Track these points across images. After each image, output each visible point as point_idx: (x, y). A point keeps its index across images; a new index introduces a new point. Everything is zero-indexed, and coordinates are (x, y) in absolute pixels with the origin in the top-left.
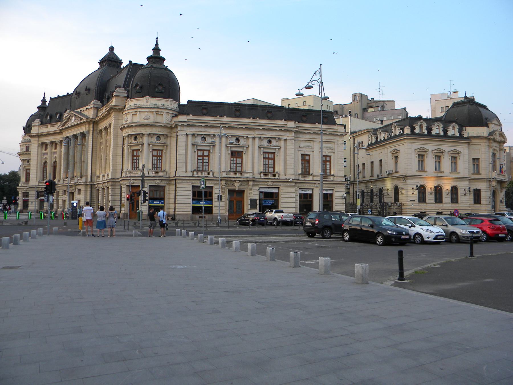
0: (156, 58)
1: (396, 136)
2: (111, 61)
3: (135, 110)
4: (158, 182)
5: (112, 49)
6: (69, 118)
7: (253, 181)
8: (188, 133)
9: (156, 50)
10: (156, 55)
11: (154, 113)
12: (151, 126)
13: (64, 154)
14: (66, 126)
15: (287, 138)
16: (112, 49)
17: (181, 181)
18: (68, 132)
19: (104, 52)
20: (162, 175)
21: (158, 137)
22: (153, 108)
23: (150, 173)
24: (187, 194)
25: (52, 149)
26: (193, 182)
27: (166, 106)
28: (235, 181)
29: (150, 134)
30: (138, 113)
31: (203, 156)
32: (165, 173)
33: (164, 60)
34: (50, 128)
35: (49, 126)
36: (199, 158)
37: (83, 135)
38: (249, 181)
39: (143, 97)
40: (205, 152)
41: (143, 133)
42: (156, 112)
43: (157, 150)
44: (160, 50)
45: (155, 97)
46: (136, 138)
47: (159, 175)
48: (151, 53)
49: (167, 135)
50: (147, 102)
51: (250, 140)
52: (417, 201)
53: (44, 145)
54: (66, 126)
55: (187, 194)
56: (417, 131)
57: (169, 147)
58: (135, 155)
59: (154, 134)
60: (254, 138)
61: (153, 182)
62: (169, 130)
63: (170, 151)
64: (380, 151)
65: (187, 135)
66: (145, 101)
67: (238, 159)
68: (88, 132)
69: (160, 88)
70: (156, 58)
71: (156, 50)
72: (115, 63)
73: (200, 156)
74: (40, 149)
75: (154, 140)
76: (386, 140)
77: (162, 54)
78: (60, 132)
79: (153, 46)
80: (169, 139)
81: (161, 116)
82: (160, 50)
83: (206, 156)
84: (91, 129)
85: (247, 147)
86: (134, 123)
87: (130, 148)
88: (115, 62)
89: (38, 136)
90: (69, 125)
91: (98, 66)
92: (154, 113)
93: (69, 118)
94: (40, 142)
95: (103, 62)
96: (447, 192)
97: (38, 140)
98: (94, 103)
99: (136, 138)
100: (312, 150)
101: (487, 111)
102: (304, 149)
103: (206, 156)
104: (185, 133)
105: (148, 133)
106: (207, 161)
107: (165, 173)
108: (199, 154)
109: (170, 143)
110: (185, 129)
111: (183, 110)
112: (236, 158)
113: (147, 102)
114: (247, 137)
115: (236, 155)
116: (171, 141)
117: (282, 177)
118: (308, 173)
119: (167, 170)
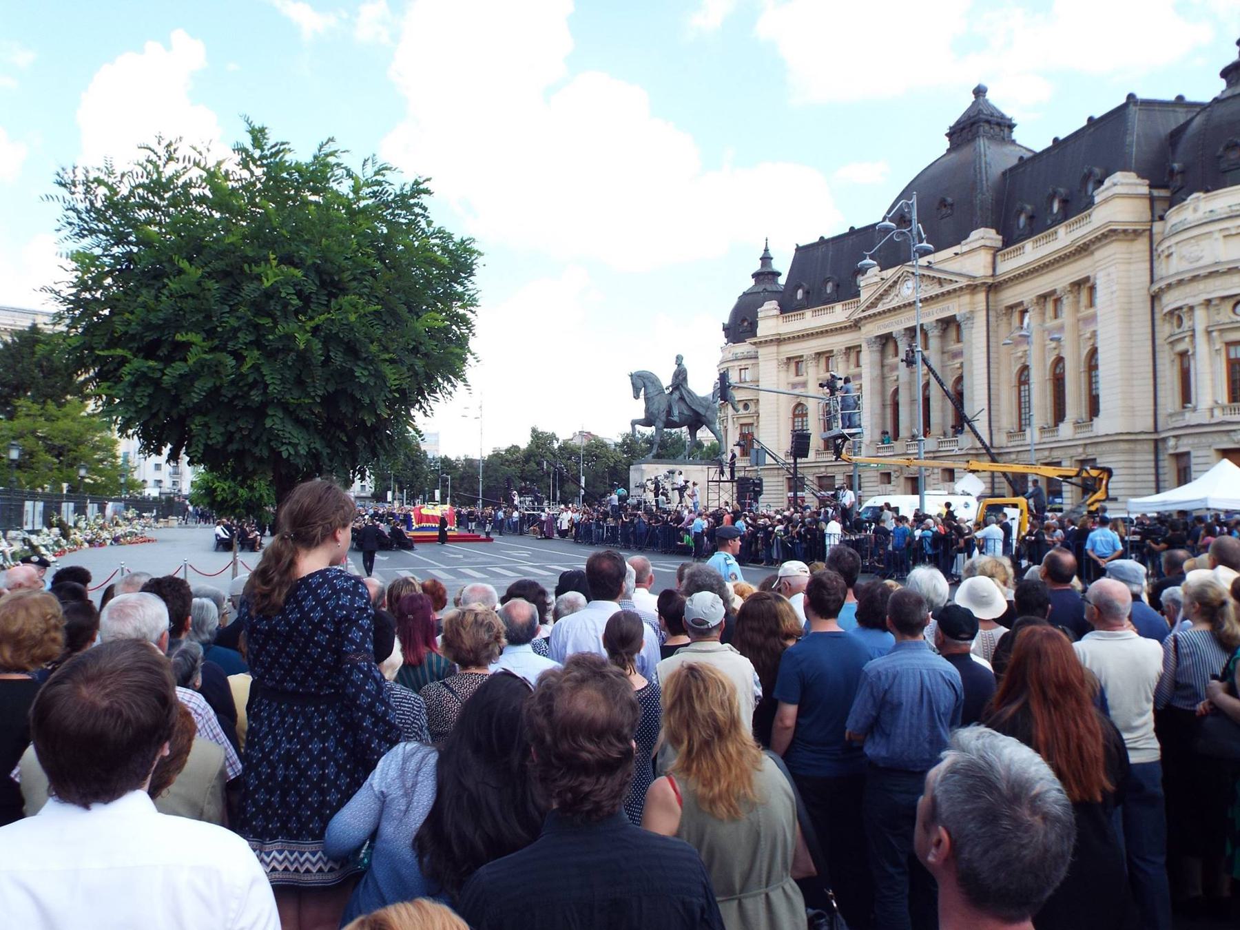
2: (979, 125)
4: (823, 469)
5: (979, 92)
6: (895, 282)
10: (764, 270)
11: (1217, 235)
13: (872, 380)
14: (880, 308)
16: (979, 92)
18: (886, 321)
23: (1217, 412)
24: (1144, 485)
25: (848, 368)
34: (810, 320)
35: (808, 313)
37: (948, 324)
53: (796, 362)
54: (880, 308)
55: (1144, 485)
58: (415, 430)
59: (1223, 298)
60: (1191, 308)
61: (1225, 438)
68: (970, 317)
72: (997, 129)
78: (856, 325)
85: (1193, 336)
86: (1172, 276)
88: (999, 124)
89: (779, 341)
90: (895, 304)
91: (946, 144)
93: (895, 282)
94: (784, 357)
95: (963, 129)
98: (985, 236)
101: (1012, 148)
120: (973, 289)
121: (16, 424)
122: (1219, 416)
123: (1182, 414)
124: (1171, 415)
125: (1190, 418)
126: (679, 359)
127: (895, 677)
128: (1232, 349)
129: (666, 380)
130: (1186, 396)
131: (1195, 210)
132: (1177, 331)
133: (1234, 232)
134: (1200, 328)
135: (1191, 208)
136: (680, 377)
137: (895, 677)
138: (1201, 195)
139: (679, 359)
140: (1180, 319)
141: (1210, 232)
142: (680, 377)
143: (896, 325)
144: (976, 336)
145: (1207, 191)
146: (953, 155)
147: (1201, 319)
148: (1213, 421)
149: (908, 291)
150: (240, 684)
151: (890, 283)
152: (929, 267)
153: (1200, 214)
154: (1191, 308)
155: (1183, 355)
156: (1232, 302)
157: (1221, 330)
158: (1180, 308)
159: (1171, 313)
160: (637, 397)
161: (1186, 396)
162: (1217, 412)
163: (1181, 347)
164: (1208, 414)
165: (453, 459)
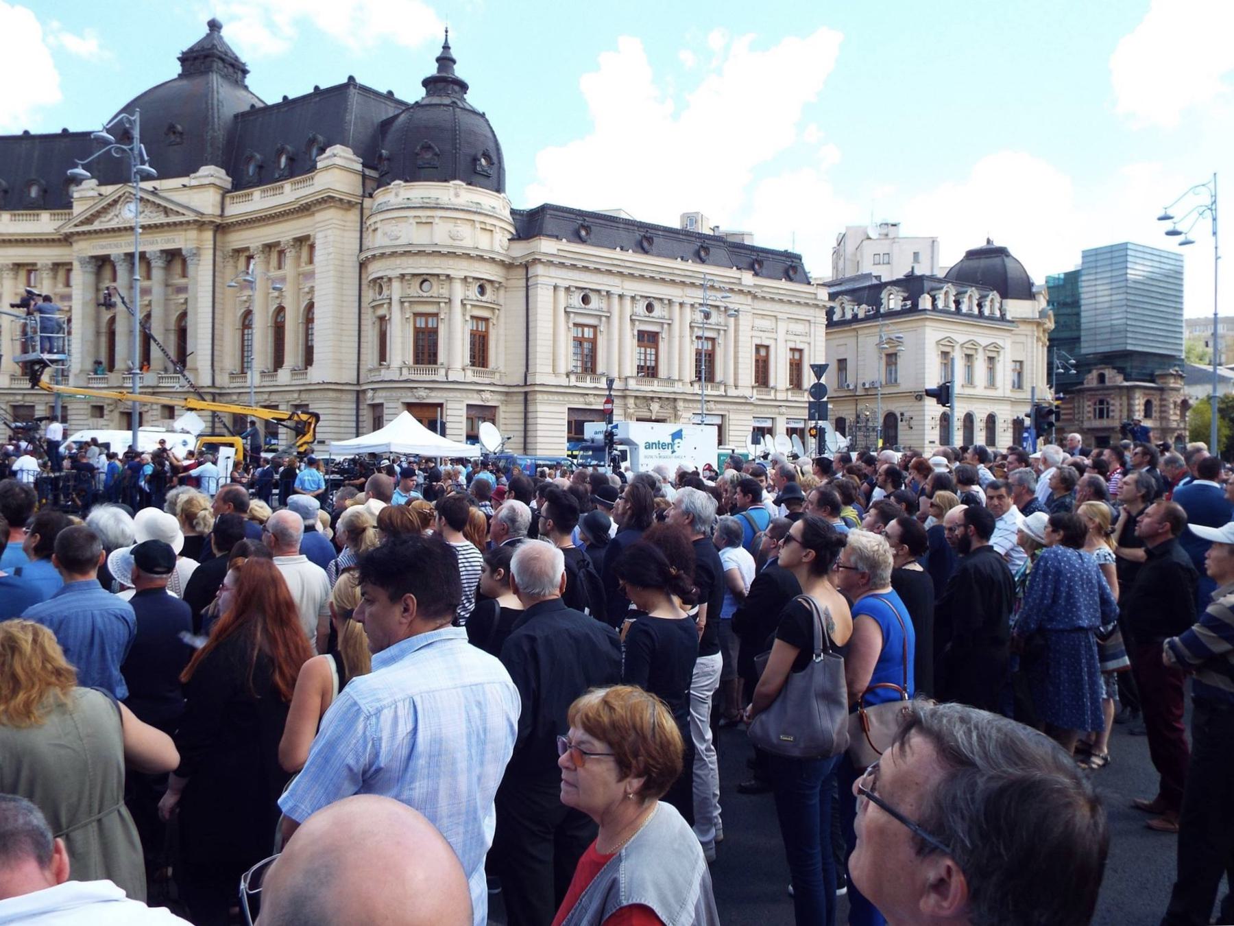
0: (444, 82)
1: (892, 314)
3: (429, 213)
5: (214, 26)
6: (115, 202)
7: (685, 400)
8: (559, 283)
9: (445, 61)
10: (444, 74)
11: (411, 220)
12: (429, 254)
13: (85, 304)
14: (96, 225)
15: (742, 308)
16: (214, 26)
17: (546, 396)
18: (104, 242)
19: (195, 34)
21: (424, 279)
23: (405, 371)
26: (571, 398)
28: (652, 398)
29: (403, 276)
30: (378, 225)
32: (497, 375)
33: (463, 87)
37: (172, 256)
38: (675, 400)
39: (446, 181)
40: (430, 320)
41: (390, 273)
43: (583, 326)
44: (454, 62)
46: (482, 290)
47: (487, 381)
48: (432, 70)
50: (457, 195)
51: (676, 308)
52: (937, 442)
54: (96, 225)
56: (940, 305)
59: (414, 275)
60: (390, 279)
64: (842, 341)
65: (555, 288)
66: (452, 192)
67: (648, 350)
68: (197, 253)
69: (428, 156)
70: (444, 82)
71: (445, 61)
72: (231, 70)
75: (473, 292)
76: (862, 320)
77: (460, 71)
79: (438, 52)
81: (428, 227)
82: (454, 62)
84: (210, 244)
85: (390, 304)
88: (232, 65)
90: (114, 224)
91: (177, 69)
93: (115, 202)
95: (195, 58)
96: (933, 423)
100: (774, 335)
102: (761, 334)
104: (554, 282)
105: (462, 274)
107: (442, 372)
110: (553, 271)
111: (530, 224)
112: (645, 348)
113: (457, 195)
114: (448, 276)
115: (648, 339)
117: (732, 392)
118: (710, 378)
120: (200, 225)
121: (484, 299)
122: (406, 375)
123: (379, 370)
124: (370, 370)
125: (386, 375)
128: (418, 319)
134: (395, 298)
140: (381, 287)
143: (116, 248)
144: (202, 274)
145: (406, 181)
146: (184, 82)
147: (396, 290)
149: (128, 213)
151: (157, 201)
152: (154, 192)
153: (400, 199)
154: (390, 279)
155: (382, 319)
158: (381, 278)
161: (383, 356)
162: (405, 371)
163: (381, 312)
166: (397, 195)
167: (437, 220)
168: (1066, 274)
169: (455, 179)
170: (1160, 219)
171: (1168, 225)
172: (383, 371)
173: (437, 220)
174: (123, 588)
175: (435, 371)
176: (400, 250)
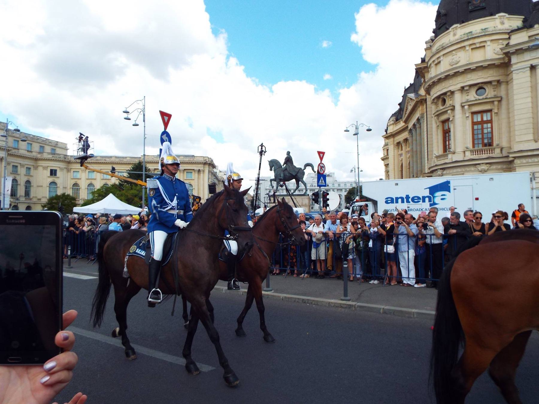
17: (524, 161)
20: (491, 155)
21: (480, 87)
22: (485, 35)
27: (491, 30)
29: (463, 88)
30: (442, 58)
31: (482, 122)
36: (476, 127)
41: (452, 88)
42: (470, 45)
45: (468, 20)
49: (498, 82)
50: (502, 23)
57: (504, 102)
59: (471, 86)
62: (501, 71)
63: (508, 109)
73: (477, 123)
74: (396, 151)
75: (472, 96)
80: (503, 87)
83: (487, 122)
85: (500, 101)
87: (438, 119)
92: (467, 48)
94: (395, 143)
97: (394, 141)
99: (444, 101)
103: (487, 122)
104: (528, 64)
105: (459, 86)
106: (489, 130)
107: (498, 151)
108: (475, 120)
109: (507, 94)
113: (502, 23)
116: (507, 90)
119: (504, 144)
122: (469, 156)
123: (447, 155)
124: (437, 157)
125: (451, 158)
126: (288, 153)
127: (95, 326)
128: (475, 116)
129: (282, 162)
130: (446, 148)
131: (455, 35)
132: (442, 108)
133: (478, 45)
135: (452, 33)
136: (289, 160)
137: (95, 326)
138: (458, 25)
139: (288, 153)
141: (464, 47)
142: (289, 160)
147: (458, 99)
148: (465, 159)
150: (306, 237)
153: (457, 37)
154: (452, 93)
156: (476, 88)
157: (469, 105)
158: (445, 94)
159: (438, 97)
160: (271, 170)
161: (446, 148)
164: (462, 154)
165: (252, 175)
166: (455, 35)
167: (489, 43)
168: (207, 10)
169: (499, 12)
170: (133, 125)
171: (125, 115)
172: (450, 156)
173: (489, 43)
174: (408, 236)
175: (493, 150)
176: (461, 70)
